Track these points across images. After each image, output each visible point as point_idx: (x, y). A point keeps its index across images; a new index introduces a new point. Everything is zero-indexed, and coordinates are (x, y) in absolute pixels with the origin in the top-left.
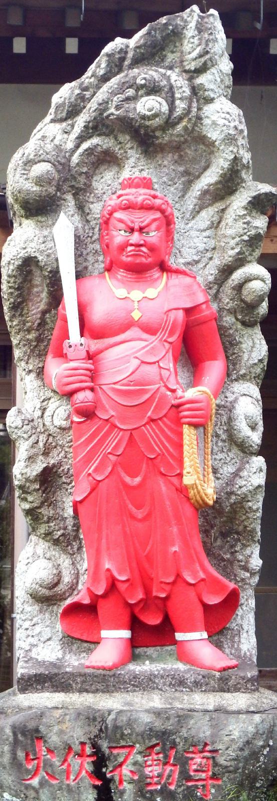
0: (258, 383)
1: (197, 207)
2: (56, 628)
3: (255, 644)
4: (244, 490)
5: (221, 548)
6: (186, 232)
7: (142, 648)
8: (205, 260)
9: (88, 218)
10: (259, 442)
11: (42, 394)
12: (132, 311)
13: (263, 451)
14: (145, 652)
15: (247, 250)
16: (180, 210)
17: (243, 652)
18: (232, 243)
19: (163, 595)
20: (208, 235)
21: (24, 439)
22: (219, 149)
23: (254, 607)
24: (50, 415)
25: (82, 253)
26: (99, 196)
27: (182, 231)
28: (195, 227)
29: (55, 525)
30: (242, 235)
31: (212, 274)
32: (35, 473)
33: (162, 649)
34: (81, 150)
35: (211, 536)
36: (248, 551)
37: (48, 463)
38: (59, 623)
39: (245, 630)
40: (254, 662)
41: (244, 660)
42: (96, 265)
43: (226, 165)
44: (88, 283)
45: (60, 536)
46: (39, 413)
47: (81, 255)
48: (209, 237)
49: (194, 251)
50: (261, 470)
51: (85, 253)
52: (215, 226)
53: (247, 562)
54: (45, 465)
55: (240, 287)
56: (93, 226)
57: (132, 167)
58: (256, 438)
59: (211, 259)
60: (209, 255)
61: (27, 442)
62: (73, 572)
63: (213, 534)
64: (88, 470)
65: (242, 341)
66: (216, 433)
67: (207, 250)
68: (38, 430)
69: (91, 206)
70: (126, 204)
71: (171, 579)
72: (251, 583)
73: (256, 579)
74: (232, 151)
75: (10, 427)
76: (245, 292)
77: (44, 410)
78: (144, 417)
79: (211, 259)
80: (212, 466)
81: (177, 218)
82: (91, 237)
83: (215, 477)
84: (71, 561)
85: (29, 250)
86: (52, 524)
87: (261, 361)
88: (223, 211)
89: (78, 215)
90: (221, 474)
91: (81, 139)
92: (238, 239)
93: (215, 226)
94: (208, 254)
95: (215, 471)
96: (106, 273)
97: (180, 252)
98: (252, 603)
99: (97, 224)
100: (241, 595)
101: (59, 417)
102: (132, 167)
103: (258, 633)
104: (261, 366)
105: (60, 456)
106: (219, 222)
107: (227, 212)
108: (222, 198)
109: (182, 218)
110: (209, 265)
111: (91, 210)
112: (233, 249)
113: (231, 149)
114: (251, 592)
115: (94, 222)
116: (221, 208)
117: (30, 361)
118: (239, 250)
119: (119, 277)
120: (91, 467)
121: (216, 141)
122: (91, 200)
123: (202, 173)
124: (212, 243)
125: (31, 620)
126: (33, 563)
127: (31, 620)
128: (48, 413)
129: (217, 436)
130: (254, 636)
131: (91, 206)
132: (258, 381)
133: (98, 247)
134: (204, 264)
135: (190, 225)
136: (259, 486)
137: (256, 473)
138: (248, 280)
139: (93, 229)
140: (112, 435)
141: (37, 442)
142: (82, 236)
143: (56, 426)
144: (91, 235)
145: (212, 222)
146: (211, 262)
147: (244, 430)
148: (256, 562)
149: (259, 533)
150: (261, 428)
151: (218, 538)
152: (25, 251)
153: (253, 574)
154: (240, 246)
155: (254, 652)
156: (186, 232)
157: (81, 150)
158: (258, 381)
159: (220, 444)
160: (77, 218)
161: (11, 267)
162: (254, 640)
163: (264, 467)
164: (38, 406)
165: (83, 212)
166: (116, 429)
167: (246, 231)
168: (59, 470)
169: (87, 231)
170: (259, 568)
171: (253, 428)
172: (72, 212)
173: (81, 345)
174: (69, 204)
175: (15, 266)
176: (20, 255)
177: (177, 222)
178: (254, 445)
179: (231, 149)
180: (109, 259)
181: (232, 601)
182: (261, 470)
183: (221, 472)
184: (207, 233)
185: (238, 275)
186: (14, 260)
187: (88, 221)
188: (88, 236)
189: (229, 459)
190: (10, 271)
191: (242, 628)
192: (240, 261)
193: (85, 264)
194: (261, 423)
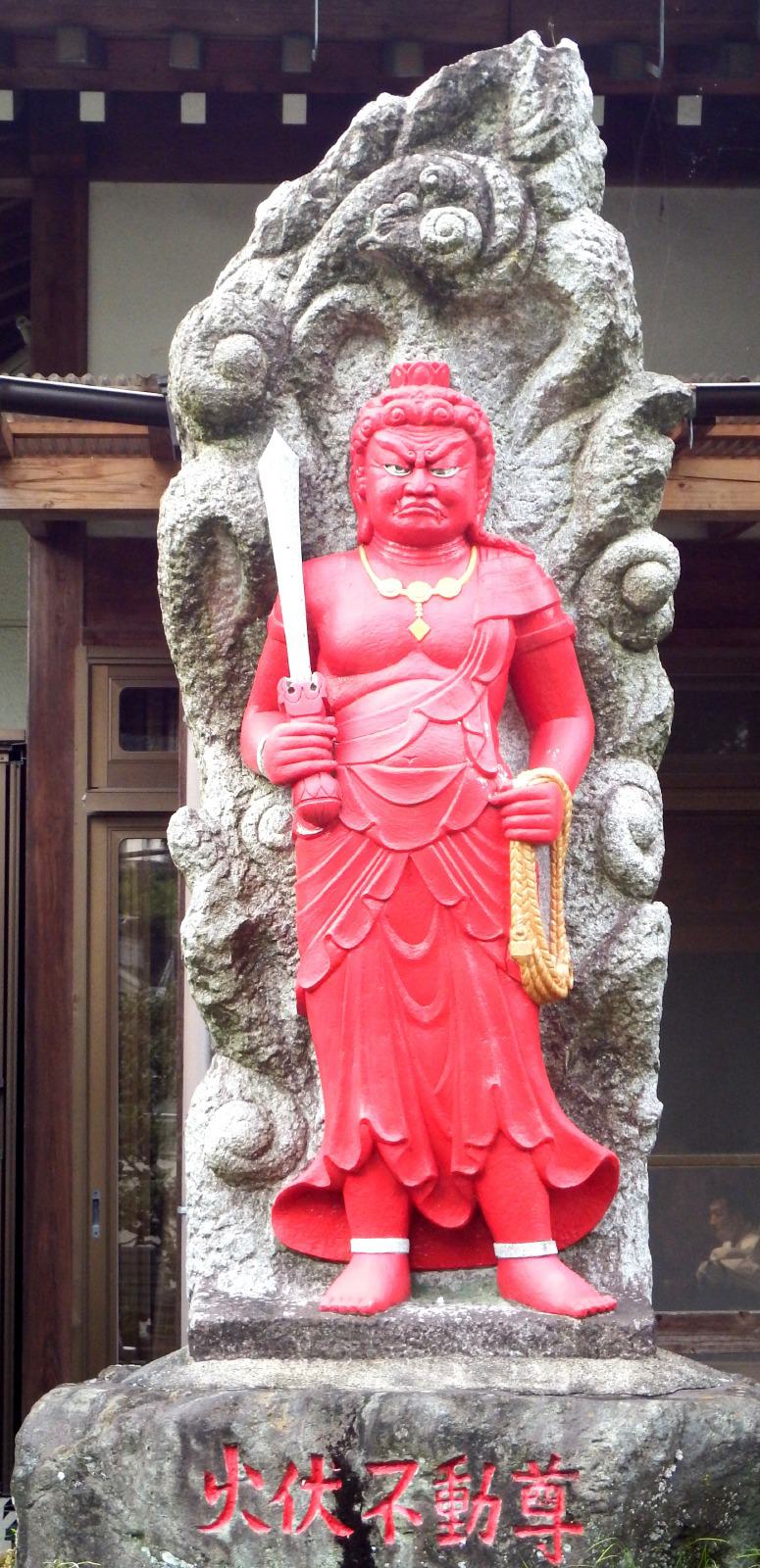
1: (537, 421)
4: (628, 967)
5: (583, 1079)
6: (514, 470)
7: (430, 1273)
8: (551, 523)
9: (325, 442)
10: (656, 874)
11: (236, 782)
12: (410, 622)
14: (437, 1281)
17: (625, 1281)
18: (605, 490)
19: (471, 1171)
21: (202, 868)
22: (578, 309)
23: (647, 1193)
25: (314, 509)
29: (262, 1035)
31: (565, 551)
32: (222, 935)
33: (470, 1274)
36: (635, 1086)
37: (249, 916)
38: (269, 1224)
39: (630, 1238)
41: (628, 1295)
44: (325, 567)
45: (272, 1056)
46: (231, 819)
48: (560, 479)
49: (531, 506)
50: (660, 929)
52: (572, 457)
53: (634, 1107)
54: (242, 919)
55: (619, 576)
57: (411, 344)
58: (650, 866)
59: (563, 521)
60: (559, 513)
61: (208, 875)
62: (296, 1126)
63: (568, 1053)
65: (624, 679)
67: (557, 504)
68: (230, 851)
69: (332, 419)
73: (651, 1139)
74: (604, 313)
75: (175, 846)
76: (629, 585)
77: (240, 813)
81: (499, 442)
83: (572, 942)
85: (211, 503)
86: (256, 1034)
87: (660, 718)
88: (587, 427)
89: (307, 436)
90: (584, 937)
91: (313, 289)
92: (616, 483)
93: (572, 457)
94: (558, 511)
95: (572, 930)
96: (362, 550)
97: (503, 507)
98: (643, 1185)
100: (622, 1170)
101: (270, 827)
102: (411, 344)
105: (272, 901)
106: (580, 451)
108: (585, 404)
109: (508, 441)
111: (331, 427)
112: (605, 501)
113: (602, 308)
114: (641, 1165)
115: (338, 450)
117: (213, 719)
118: (618, 503)
119: (386, 555)
122: (332, 407)
123: (547, 355)
128: (248, 819)
129: (576, 863)
130: (647, 1250)
131: (332, 419)
134: (550, 531)
135: (522, 456)
136: (657, 960)
137: (650, 935)
138: (635, 562)
141: (227, 875)
142: (314, 477)
144: (331, 474)
146: (563, 528)
147: (626, 850)
148: (651, 1107)
149: (657, 1051)
150: (660, 849)
151: (576, 1059)
152: (204, 505)
153: (644, 1130)
155: (646, 1280)
158: (655, 757)
159: (581, 878)
160: (304, 442)
161: (178, 537)
162: (646, 1257)
163: (667, 923)
165: (317, 430)
169: (324, 467)
171: (645, 847)
172: (295, 431)
173: (313, 687)
174: (290, 415)
178: (646, 881)
179: (602, 308)
181: (604, 1182)
182: (660, 929)
183: (584, 934)
184: (557, 471)
185: (615, 553)
187: (325, 448)
192: (619, 526)
194: (660, 838)
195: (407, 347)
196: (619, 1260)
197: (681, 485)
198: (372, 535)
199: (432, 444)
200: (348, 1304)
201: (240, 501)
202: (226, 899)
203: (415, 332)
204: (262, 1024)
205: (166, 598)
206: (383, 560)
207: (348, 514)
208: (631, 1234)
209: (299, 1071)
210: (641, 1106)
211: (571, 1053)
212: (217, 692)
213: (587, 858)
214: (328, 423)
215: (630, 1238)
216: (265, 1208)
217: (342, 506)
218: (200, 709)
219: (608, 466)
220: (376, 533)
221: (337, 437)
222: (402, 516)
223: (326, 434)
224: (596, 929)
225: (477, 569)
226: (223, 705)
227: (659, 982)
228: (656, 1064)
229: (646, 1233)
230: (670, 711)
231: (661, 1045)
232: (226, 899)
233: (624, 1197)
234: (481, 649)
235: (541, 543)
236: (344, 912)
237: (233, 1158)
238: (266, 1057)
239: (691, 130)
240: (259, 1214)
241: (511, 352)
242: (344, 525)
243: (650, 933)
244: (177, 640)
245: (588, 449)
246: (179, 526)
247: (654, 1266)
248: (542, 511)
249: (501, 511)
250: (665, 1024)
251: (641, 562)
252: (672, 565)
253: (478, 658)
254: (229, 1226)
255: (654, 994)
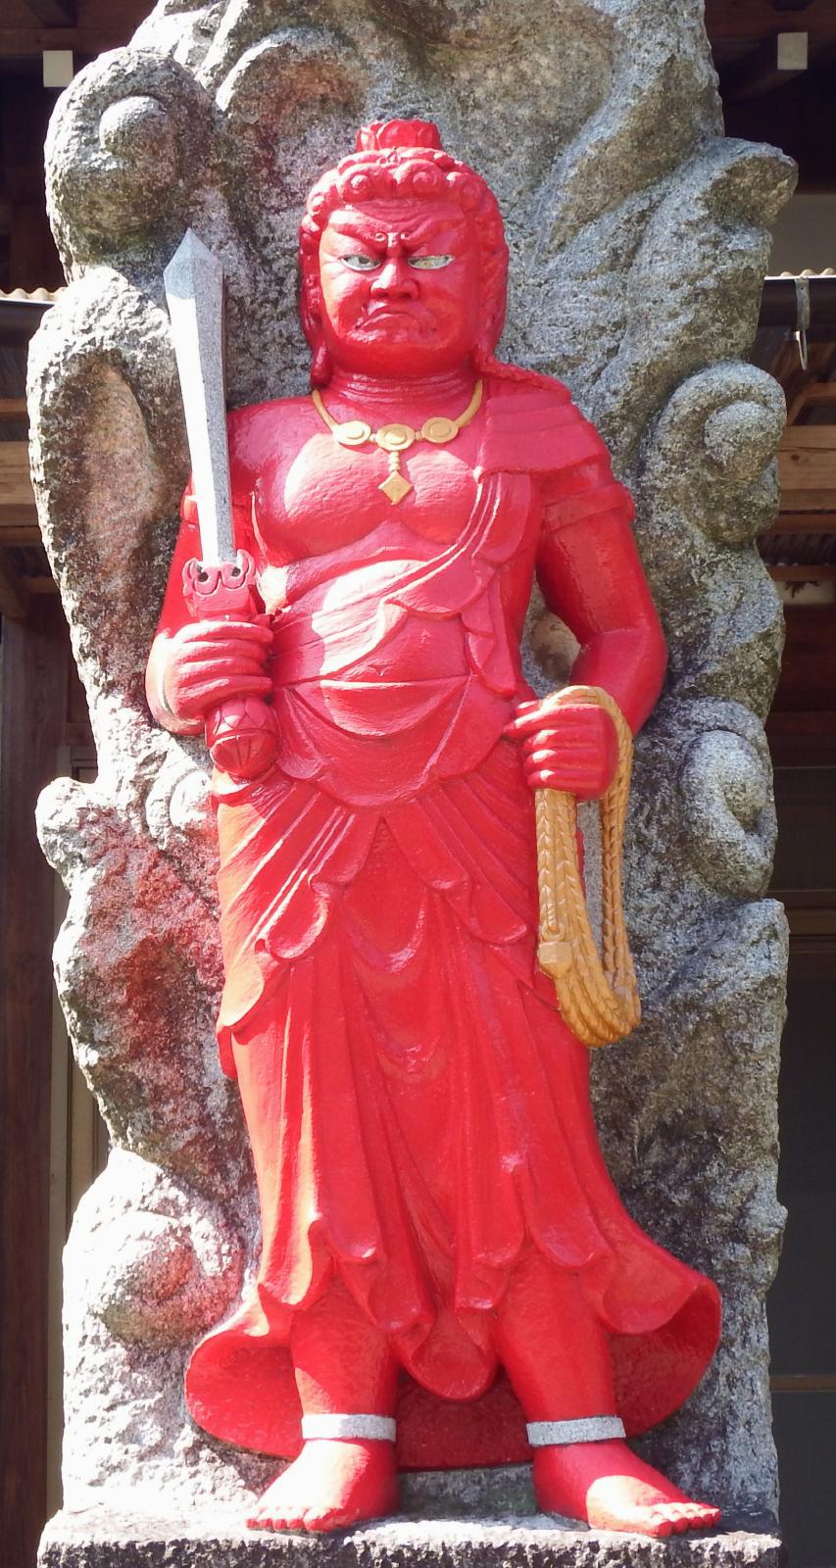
0: (760, 706)
1: (571, 215)
2: (176, 1415)
3: (774, 1461)
4: (726, 995)
5: (662, 1170)
6: (540, 285)
7: (430, 1474)
8: (594, 358)
9: (265, 252)
10: (766, 861)
11: (142, 744)
12: (383, 477)
13: (778, 885)
14: (442, 1487)
15: (714, 320)
16: (521, 226)
17: (736, 1484)
18: (672, 299)
19: (487, 1305)
20: (602, 286)
21: (83, 861)
22: (626, 40)
23: (766, 1348)
24: (163, 796)
25: (248, 343)
26: (296, 189)
27: (531, 281)
28: (565, 268)
29: (174, 1111)
30: (697, 277)
31: (615, 393)
32: (112, 959)
33: (492, 1476)
34: (243, 63)
35: (631, 1135)
36: (745, 1182)
37: (153, 930)
38: (185, 1400)
39: (742, 1419)
40: (769, 1513)
41: (740, 1507)
42: (288, 376)
43: (650, 82)
44: (270, 424)
45: (189, 1143)
46: (130, 794)
47: (245, 349)
48: (605, 292)
49: (564, 333)
50: (775, 935)
51: (255, 345)
52: (622, 260)
53: (743, 1213)
54: (140, 936)
55: (697, 425)
56: (281, 275)
57: (385, 106)
58: (756, 853)
59: (613, 352)
60: (607, 342)
61: (92, 871)
62: (225, 1248)
63: (637, 1130)
64: (258, 933)
65: (710, 583)
66: (639, 834)
67: (603, 329)
68: (127, 839)
69: (274, 219)
70: (361, 184)
71: (506, 1255)
72: (757, 1277)
73: (769, 1267)
74: (662, 44)
75: (47, 830)
76: (714, 437)
77: (144, 788)
78: (416, 770)
79: (613, 352)
80: (629, 931)
81: (516, 246)
82: (275, 303)
83: (637, 961)
84: (221, 1216)
85: (97, 334)
86: (167, 1109)
87: (765, 637)
88: (643, 217)
89: (238, 245)
90: (657, 954)
91: (241, 37)
92: (686, 288)
93: (622, 260)
94: (604, 339)
95: (638, 944)
96: (316, 396)
97: (524, 337)
98: (761, 1336)
99: (290, 267)
100: (727, 1312)
101: (187, 802)
102: (385, 106)
103: (781, 1432)
104: (767, 654)
105: (190, 910)
106: (635, 250)
107: (655, 218)
108: (640, 186)
109: (530, 246)
110: (607, 369)
111: (273, 231)
112: (673, 315)
113: (659, 36)
114: (754, 1303)
115: (282, 262)
116: (637, 209)
117: (111, 657)
118: (691, 317)
119: (349, 395)
120: (266, 920)
121: (616, 19)
122: (274, 202)
123: (583, 121)
124: (617, 308)
125: (105, 1391)
126: (116, 1225)
127: (105, 1391)
128: (157, 792)
129: (642, 842)
130: (770, 1438)
131: (274, 219)
132: (760, 699)
133: (296, 328)
134: (594, 368)
135: (551, 265)
136: (771, 980)
137: (756, 954)
138: (722, 401)
139: (281, 281)
140: (328, 824)
141: (122, 871)
142: (249, 300)
143: (177, 829)
144: (273, 295)
145: (614, 251)
146: (613, 362)
147: (722, 825)
148: (769, 1215)
149: (775, 1128)
150: (772, 827)
151: (651, 1141)
152: (88, 337)
153: (758, 1249)
154: (695, 306)
155: (770, 1488)
156: (540, 285)
157: (243, 63)
158: (760, 699)
159: (652, 865)
160: (233, 252)
161: (51, 386)
162: (768, 1449)
163: (782, 925)
164: (131, 774)
165: (254, 239)
166: (337, 809)
167: (708, 263)
168: (186, 951)
169: (262, 286)
170: (777, 1231)
171: (752, 825)
172: (221, 236)
173: (236, 571)
174: (214, 216)
175: (60, 382)
176: (76, 350)
177: (515, 258)
178: (749, 868)
179: (659, 36)
180: (322, 351)
181: (695, 1327)
182: (775, 935)
183: (656, 947)
184: (599, 283)
185: (689, 394)
186: (58, 364)
187: (267, 262)
188: (267, 301)
189: (677, 910)
190: (48, 396)
191: (731, 1412)
192: (692, 360)
193: (256, 374)
194: (771, 812)
195: (380, 111)
196: (724, 1452)
197: (795, 458)
198: (332, 373)
199: (412, 222)
200: (290, 1516)
201: (137, 327)
202: (120, 907)
203: (390, 90)
204: (174, 1094)
205: (40, 484)
206: (345, 401)
207: (300, 351)
208: (743, 1413)
209: (230, 1165)
210: (753, 1212)
211: (642, 1130)
212: (115, 618)
213: (659, 835)
214: (269, 225)
215: (742, 1419)
216: (179, 1374)
217: (289, 339)
218: (92, 644)
219: (674, 266)
220: (336, 368)
221: (281, 244)
222: (367, 329)
223: (266, 239)
224: (670, 943)
225: (483, 407)
226: (124, 637)
227: (775, 1014)
228: (774, 1147)
229: (767, 1410)
230: (778, 630)
231: (783, 1116)
232: (120, 907)
233: (733, 1356)
234: (490, 512)
235: (581, 386)
236: (287, 900)
237: (128, 1298)
238: (181, 1144)
239: (798, 75)
240: (169, 1384)
241: (531, 119)
242: (292, 366)
243: (758, 942)
244: (56, 546)
245: (645, 245)
246: (53, 370)
247: (781, 1463)
248: (580, 338)
249: (520, 340)
250: (785, 1080)
251: (729, 401)
252: (775, 406)
253: (484, 526)
254: (125, 1403)
255: (766, 1040)
